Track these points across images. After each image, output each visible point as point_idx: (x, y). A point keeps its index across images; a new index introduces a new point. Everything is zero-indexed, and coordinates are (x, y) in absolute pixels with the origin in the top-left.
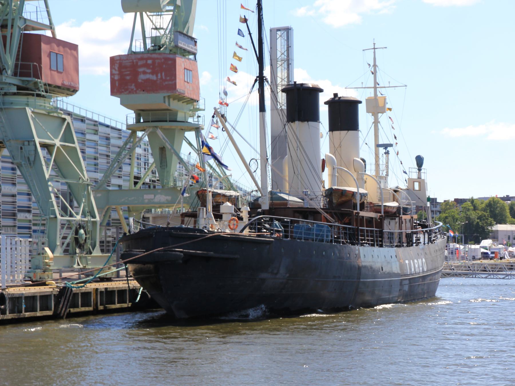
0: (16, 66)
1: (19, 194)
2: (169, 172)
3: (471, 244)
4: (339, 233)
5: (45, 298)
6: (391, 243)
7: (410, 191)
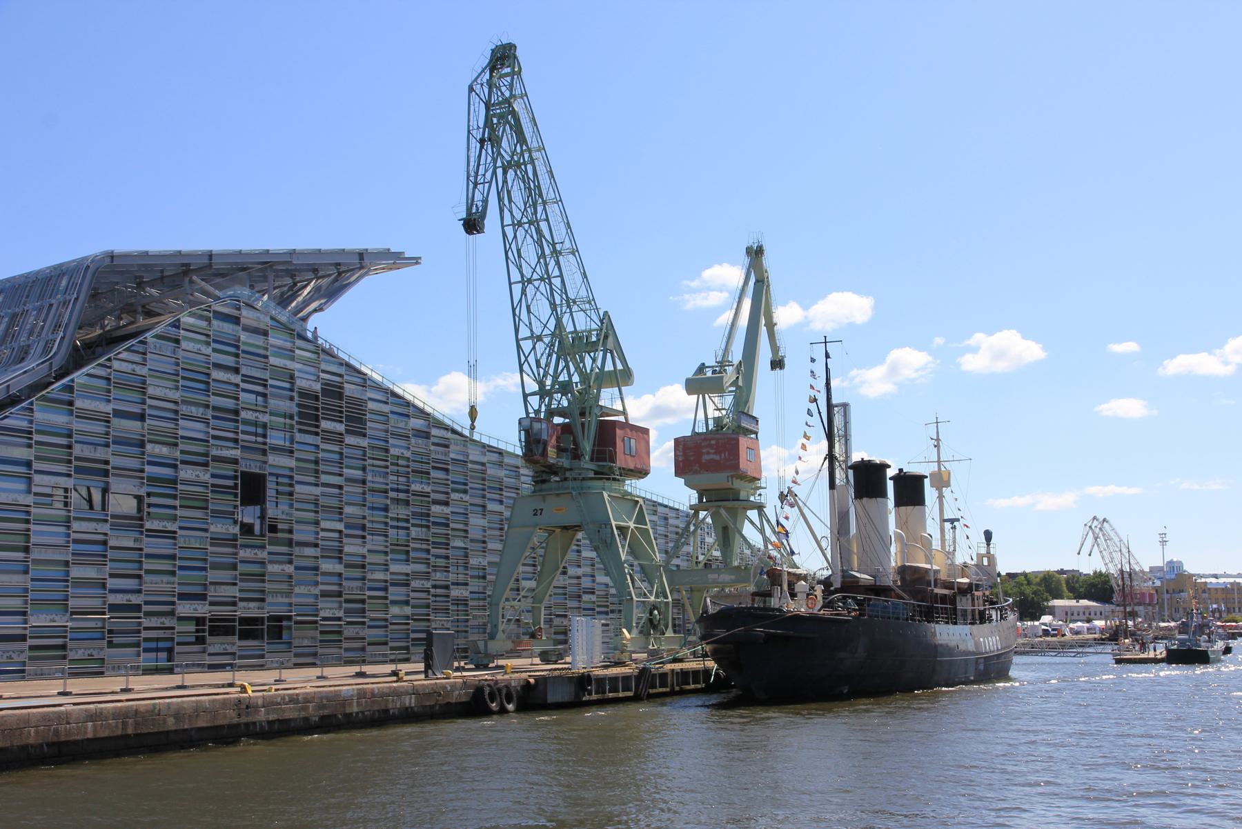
0: (593, 451)
1: (584, 575)
2: (732, 551)
3: (1027, 621)
4: (914, 611)
5: (626, 679)
6: (964, 620)
7: (979, 566)
